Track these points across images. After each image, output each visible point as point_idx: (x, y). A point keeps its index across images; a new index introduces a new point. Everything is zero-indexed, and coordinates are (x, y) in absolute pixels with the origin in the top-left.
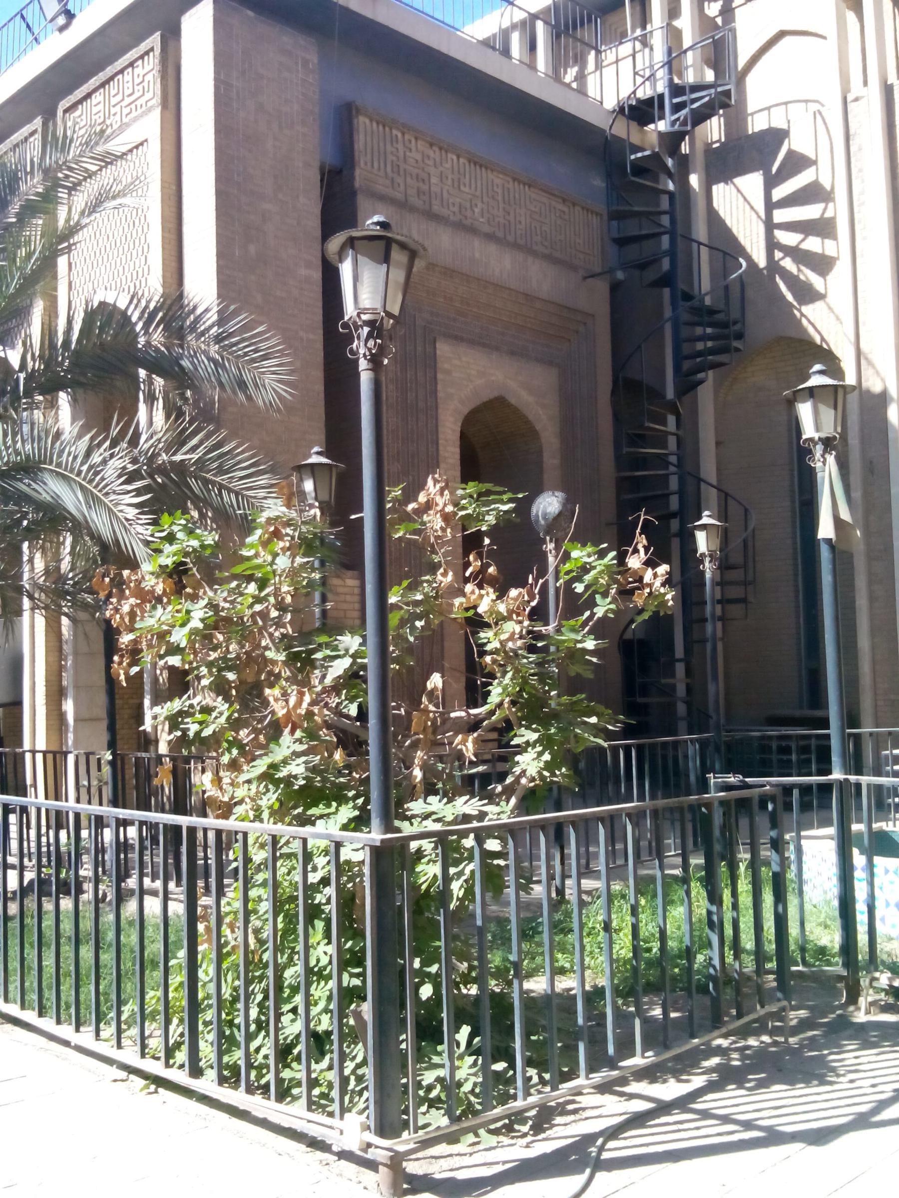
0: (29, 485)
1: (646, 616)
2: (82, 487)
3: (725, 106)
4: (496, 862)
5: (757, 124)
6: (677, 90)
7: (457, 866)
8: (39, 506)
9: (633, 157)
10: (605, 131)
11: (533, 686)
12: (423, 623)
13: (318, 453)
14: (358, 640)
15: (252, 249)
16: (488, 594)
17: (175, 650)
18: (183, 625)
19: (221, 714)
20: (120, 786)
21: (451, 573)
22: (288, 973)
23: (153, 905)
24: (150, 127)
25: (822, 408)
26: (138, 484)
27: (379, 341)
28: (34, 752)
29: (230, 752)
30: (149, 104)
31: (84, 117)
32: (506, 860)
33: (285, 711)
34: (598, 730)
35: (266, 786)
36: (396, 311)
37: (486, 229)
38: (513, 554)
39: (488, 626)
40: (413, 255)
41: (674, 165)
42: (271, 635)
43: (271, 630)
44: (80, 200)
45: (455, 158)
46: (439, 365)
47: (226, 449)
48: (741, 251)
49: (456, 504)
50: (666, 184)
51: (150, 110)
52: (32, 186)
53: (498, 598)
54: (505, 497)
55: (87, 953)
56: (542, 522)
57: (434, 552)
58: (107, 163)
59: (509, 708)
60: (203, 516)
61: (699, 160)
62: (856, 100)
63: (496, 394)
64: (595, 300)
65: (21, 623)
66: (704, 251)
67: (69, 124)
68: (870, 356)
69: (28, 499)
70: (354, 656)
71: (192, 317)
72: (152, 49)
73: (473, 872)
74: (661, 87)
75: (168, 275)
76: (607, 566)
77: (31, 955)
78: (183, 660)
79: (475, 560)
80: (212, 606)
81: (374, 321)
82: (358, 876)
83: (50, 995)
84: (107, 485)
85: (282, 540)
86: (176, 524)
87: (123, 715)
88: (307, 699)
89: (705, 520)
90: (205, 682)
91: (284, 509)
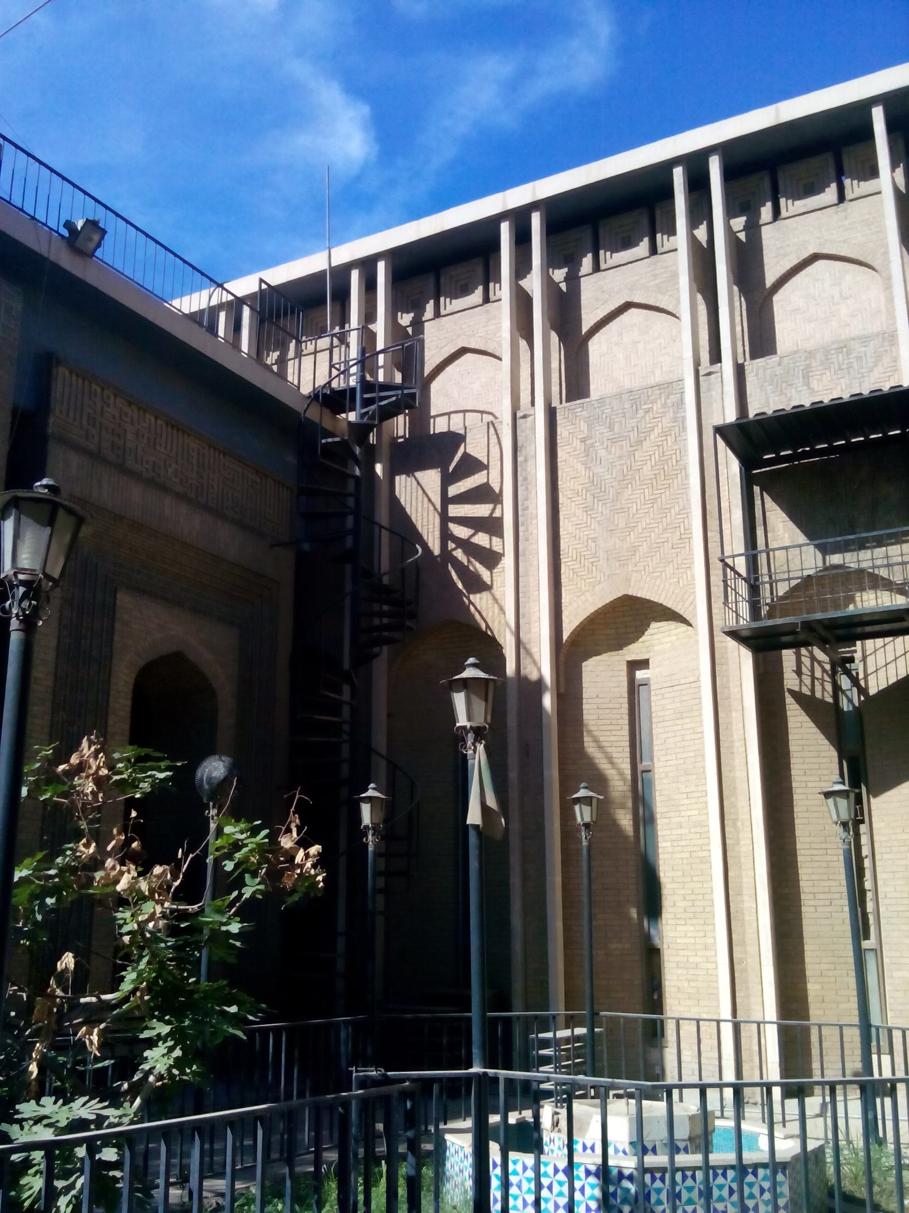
1: (296, 897)
3: (411, 407)
4: (111, 1173)
5: (439, 426)
6: (367, 386)
9: (323, 441)
10: (299, 414)
11: (170, 972)
25: (474, 698)
32: (122, 1171)
34: (238, 1020)
36: (56, 574)
38: (164, 828)
41: (360, 453)
45: (153, 418)
48: (418, 538)
49: (111, 767)
50: (354, 471)
53: (140, 874)
54: (163, 765)
56: (206, 787)
61: (385, 450)
62: (525, 417)
64: (281, 567)
66: (385, 535)
68: (528, 646)
74: (353, 382)
76: (258, 845)
79: (119, 833)
81: (32, 582)
89: (371, 793)
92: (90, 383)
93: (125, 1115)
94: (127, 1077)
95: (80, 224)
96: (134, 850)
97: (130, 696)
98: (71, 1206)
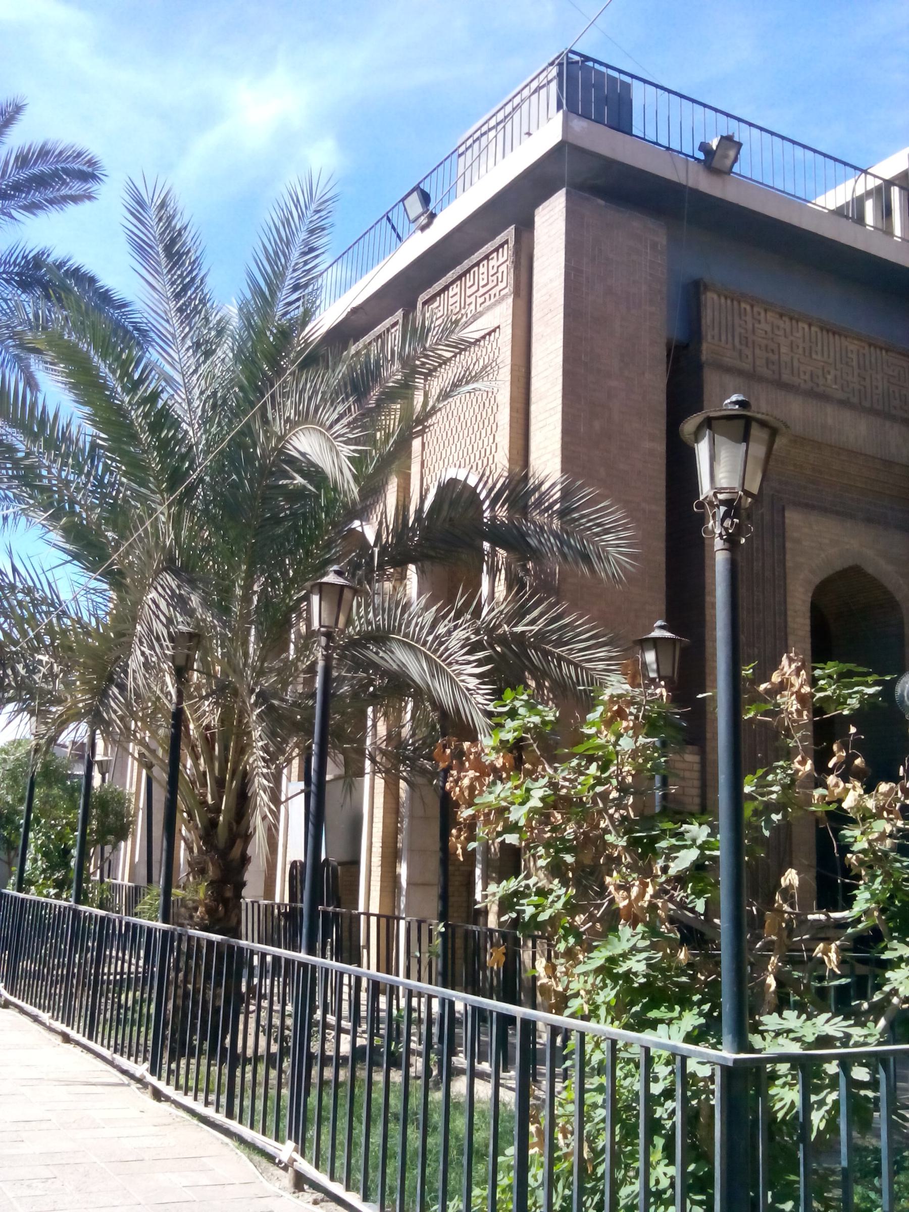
0: (377, 653)
2: (427, 657)
7: (817, 1094)
8: (385, 673)
12: (779, 817)
13: (661, 627)
14: (706, 830)
15: (597, 425)
16: (854, 788)
17: (513, 828)
18: (523, 804)
19: (559, 897)
20: (450, 956)
21: (809, 762)
22: (624, 1192)
23: (483, 1090)
24: (502, 315)
26: (480, 655)
27: (736, 520)
28: (368, 915)
29: (566, 941)
30: (503, 293)
31: (441, 308)
33: (626, 902)
35: (603, 980)
36: (755, 490)
37: (839, 395)
39: (853, 821)
40: (774, 432)
42: (611, 817)
43: (611, 811)
44: (436, 386)
45: (806, 327)
46: (787, 534)
47: (567, 620)
51: (503, 298)
52: (393, 373)
54: (870, 679)
55: (414, 1136)
57: (789, 735)
58: (462, 350)
59: (879, 917)
60: (540, 686)
63: (850, 563)
65: (363, 782)
67: (427, 315)
69: (376, 666)
70: (701, 848)
71: (537, 495)
72: (506, 242)
73: (836, 1103)
75: (515, 452)
77: (360, 1129)
78: (521, 839)
79: (840, 750)
80: (553, 785)
81: (732, 500)
82: (704, 1092)
83: (375, 1176)
84: (450, 655)
85: (626, 720)
86: (518, 700)
87: (456, 881)
88: (650, 890)
90: (542, 863)
91: (627, 687)
92: (739, 303)
93: (870, 1035)
94: (864, 996)
95: (714, 144)
96: (857, 766)
97: (808, 614)
98: (824, 1121)
